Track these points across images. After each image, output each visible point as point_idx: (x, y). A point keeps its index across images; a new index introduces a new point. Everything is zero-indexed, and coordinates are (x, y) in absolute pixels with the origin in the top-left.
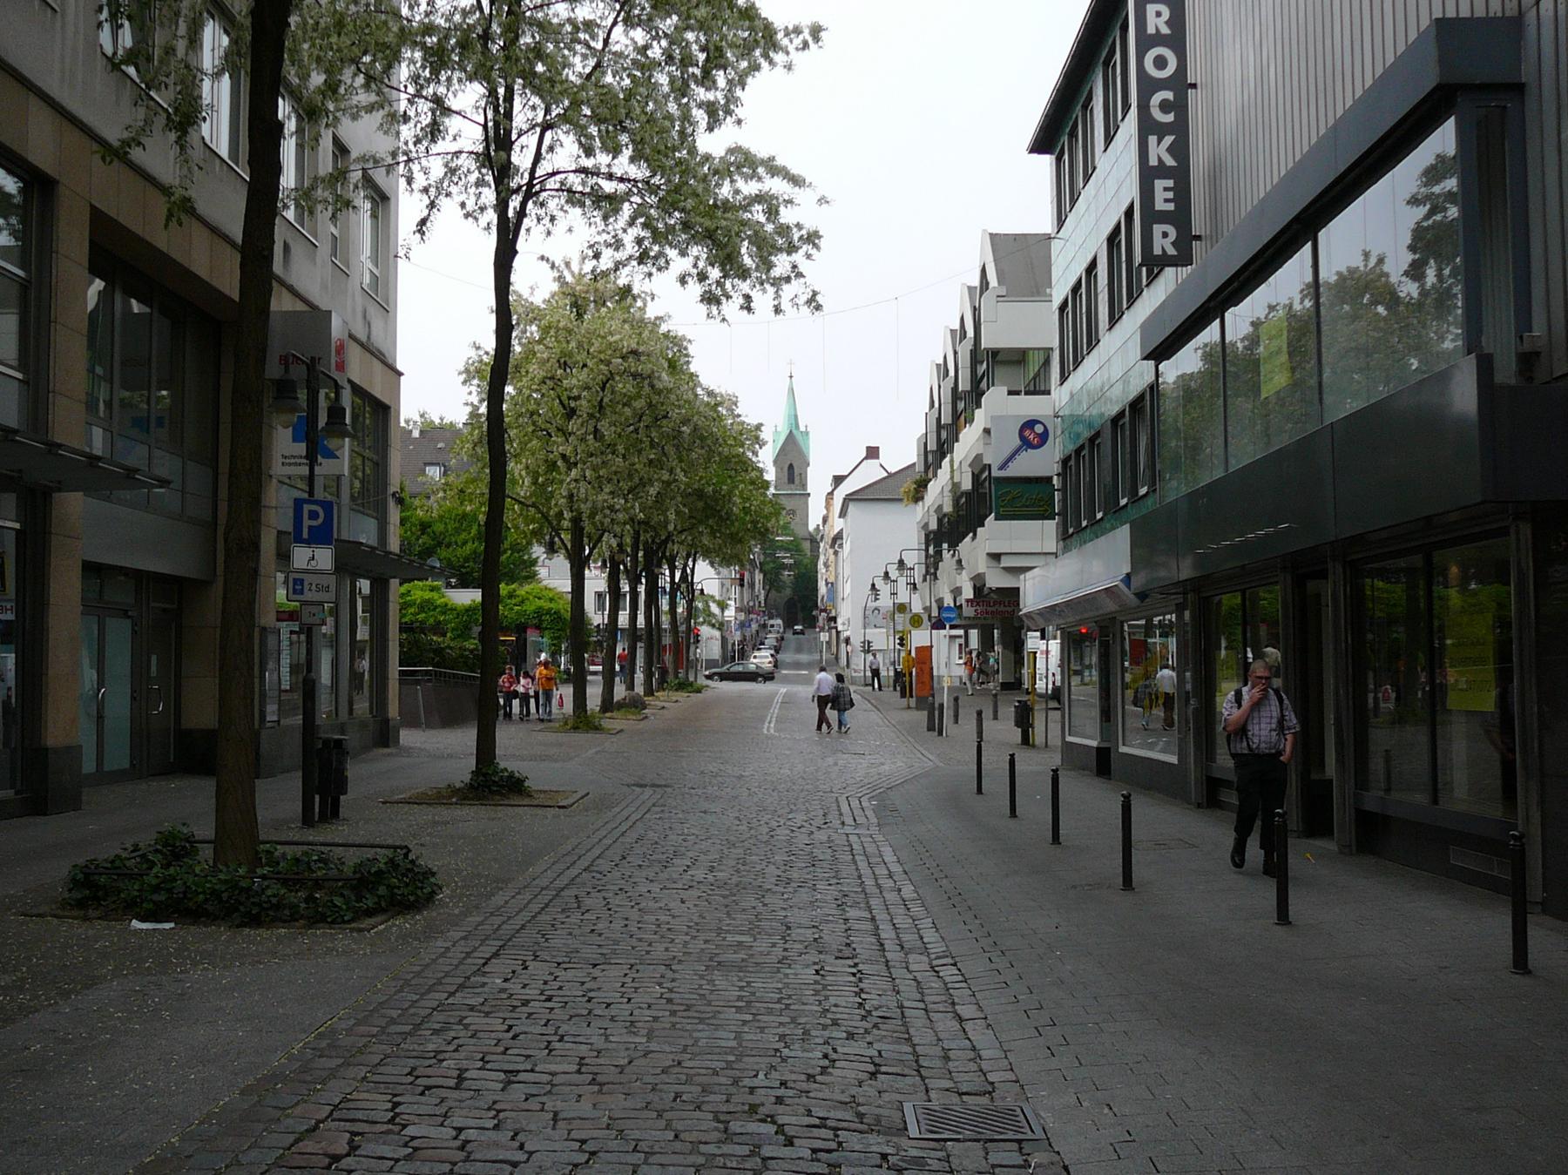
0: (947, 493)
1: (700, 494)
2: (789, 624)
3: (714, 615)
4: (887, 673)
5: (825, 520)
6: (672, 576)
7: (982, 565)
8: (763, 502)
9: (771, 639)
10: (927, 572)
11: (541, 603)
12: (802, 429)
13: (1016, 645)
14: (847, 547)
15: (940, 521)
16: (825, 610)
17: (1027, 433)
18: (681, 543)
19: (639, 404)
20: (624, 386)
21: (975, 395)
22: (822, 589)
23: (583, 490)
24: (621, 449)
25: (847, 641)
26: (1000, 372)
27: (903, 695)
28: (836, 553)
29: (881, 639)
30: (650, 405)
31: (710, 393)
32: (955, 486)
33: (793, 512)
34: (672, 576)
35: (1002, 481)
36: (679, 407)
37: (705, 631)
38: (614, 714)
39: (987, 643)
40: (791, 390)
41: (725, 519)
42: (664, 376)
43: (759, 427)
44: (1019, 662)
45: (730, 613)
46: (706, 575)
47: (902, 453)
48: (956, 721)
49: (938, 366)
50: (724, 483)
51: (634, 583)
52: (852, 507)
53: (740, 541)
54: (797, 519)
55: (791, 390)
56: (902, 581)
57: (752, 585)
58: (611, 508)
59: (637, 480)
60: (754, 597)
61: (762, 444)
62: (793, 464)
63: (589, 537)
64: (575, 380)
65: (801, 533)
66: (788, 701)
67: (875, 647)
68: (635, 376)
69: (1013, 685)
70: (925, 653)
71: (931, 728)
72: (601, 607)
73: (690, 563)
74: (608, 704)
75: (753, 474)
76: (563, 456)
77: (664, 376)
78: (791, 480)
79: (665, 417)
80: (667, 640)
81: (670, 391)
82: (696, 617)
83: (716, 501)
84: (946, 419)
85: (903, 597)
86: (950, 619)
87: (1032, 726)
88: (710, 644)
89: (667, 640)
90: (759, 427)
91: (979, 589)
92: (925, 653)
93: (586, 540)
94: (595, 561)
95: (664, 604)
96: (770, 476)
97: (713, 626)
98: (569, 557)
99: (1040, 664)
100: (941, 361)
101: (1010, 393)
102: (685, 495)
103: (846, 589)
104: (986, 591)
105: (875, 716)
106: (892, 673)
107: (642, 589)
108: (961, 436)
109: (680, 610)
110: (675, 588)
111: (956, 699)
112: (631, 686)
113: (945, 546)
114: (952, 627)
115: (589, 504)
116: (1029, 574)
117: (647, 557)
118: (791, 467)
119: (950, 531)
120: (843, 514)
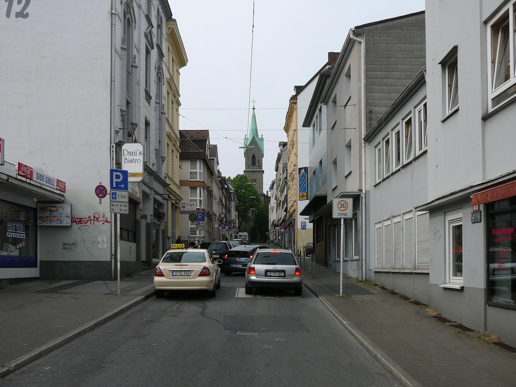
12: (260, 137)
40: (254, 116)
55: (254, 116)
78: (254, 163)
118: (254, 156)
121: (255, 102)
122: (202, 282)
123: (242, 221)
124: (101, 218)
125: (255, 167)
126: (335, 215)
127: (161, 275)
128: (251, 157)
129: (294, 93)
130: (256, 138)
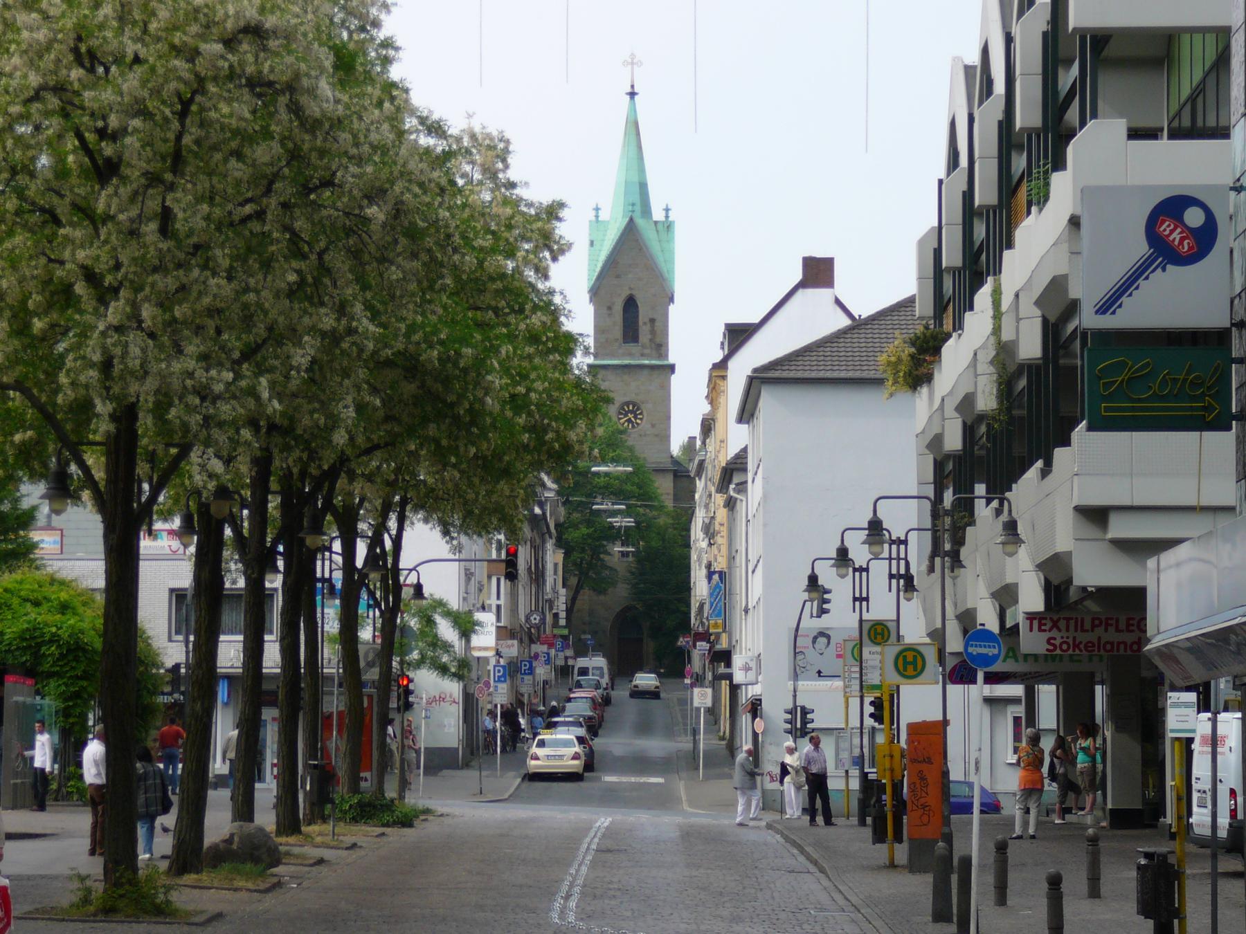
0: (984, 367)
1: (410, 365)
2: (623, 667)
3: (447, 647)
4: (843, 784)
5: (707, 426)
6: (349, 553)
7: (1064, 536)
8: (560, 386)
9: (580, 705)
10: (936, 551)
11: (33, 614)
12: (658, 215)
13: (1145, 722)
14: (755, 490)
15: (969, 431)
16: (705, 636)
17: (1165, 227)
18: (370, 478)
19: (264, 153)
20: (233, 109)
21: (1052, 140)
22: (700, 587)
23: (135, 351)
24: (222, 256)
25: (755, 708)
26: (1109, 84)
27: (879, 836)
28: (730, 504)
29: (832, 703)
30: (295, 155)
31: (436, 129)
32: (1004, 350)
33: (632, 409)
34: (349, 553)
35: (1107, 339)
36: (360, 161)
37: (426, 681)
38: (205, 877)
39: (1077, 716)
40: (633, 128)
41: (473, 421)
42: (325, 87)
43: (553, 211)
44: (1153, 764)
45: (485, 640)
46: (430, 556)
47: (883, 275)
48: (1001, 899)
49: (969, 70)
50: (464, 341)
51: (259, 564)
52: (768, 400)
53: (507, 473)
54: (644, 425)
55: (633, 128)
56: (880, 571)
57: (537, 576)
58: (204, 393)
59: (260, 330)
60: (543, 604)
61: (559, 251)
62: (635, 294)
63: (152, 458)
64: (108, 96)
65: (651, 456)
66: (613, 848)
67: (819, 720)
68: (257, 84)
69: (1141, 816)
70: (931, 737)
71: (941, 915)
72: (179, 626)
73: (392, 524)
74: (190, 855)
75: (537, 319)
76: (91, 276)
77: (325, 87)
78: (630, 332)
79: (328, 183)
80: (334, 703)
81: (338, 123)
82: (404, 651)
83: (446, 381)
84: (985, 194)
85: (882, 606)
86: (986, 660)
87: (1179, 913)
88: (437, 707)
89: (334, 703)
90: (553, 211)
91: (1057, 587)
92: (931, 737)
93: (142, 468)
94: (166, 516)
95: (330, 618)
96: (580, 319)
97: (443, 670)
98: (102, 504)
99: (1201, 766)
100: (974, 58)
101: (1135, 134)
102: (379, 364)
103: (753, 587)
104: (1073, 595)
105: (812, 886)
106: (855, 784)
107: (275, 582)
108: (1020, 234)
109: (366, 634)
110: (354, 581)
111: (1002, 848)
112: (244, 808)
113: (980, 489)
114: (992, 679)
115: (151, 384)
116: (1168, 557)
117: (288, 512)
118: (630, 305)
119: (985, 461)
120: (747, 413)
121: (640, 64)
122: (576, 765)
123: (577, 592)
124: (448, 698)
125: (632, 347)
126: (696, 703)
127: (537, 758)
128: (619, 307)
129: (718, 356)
130: (640, 222)
